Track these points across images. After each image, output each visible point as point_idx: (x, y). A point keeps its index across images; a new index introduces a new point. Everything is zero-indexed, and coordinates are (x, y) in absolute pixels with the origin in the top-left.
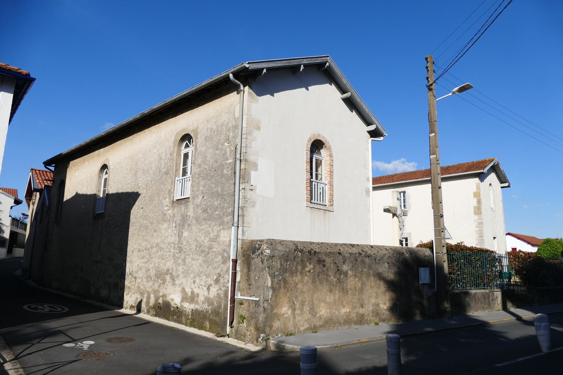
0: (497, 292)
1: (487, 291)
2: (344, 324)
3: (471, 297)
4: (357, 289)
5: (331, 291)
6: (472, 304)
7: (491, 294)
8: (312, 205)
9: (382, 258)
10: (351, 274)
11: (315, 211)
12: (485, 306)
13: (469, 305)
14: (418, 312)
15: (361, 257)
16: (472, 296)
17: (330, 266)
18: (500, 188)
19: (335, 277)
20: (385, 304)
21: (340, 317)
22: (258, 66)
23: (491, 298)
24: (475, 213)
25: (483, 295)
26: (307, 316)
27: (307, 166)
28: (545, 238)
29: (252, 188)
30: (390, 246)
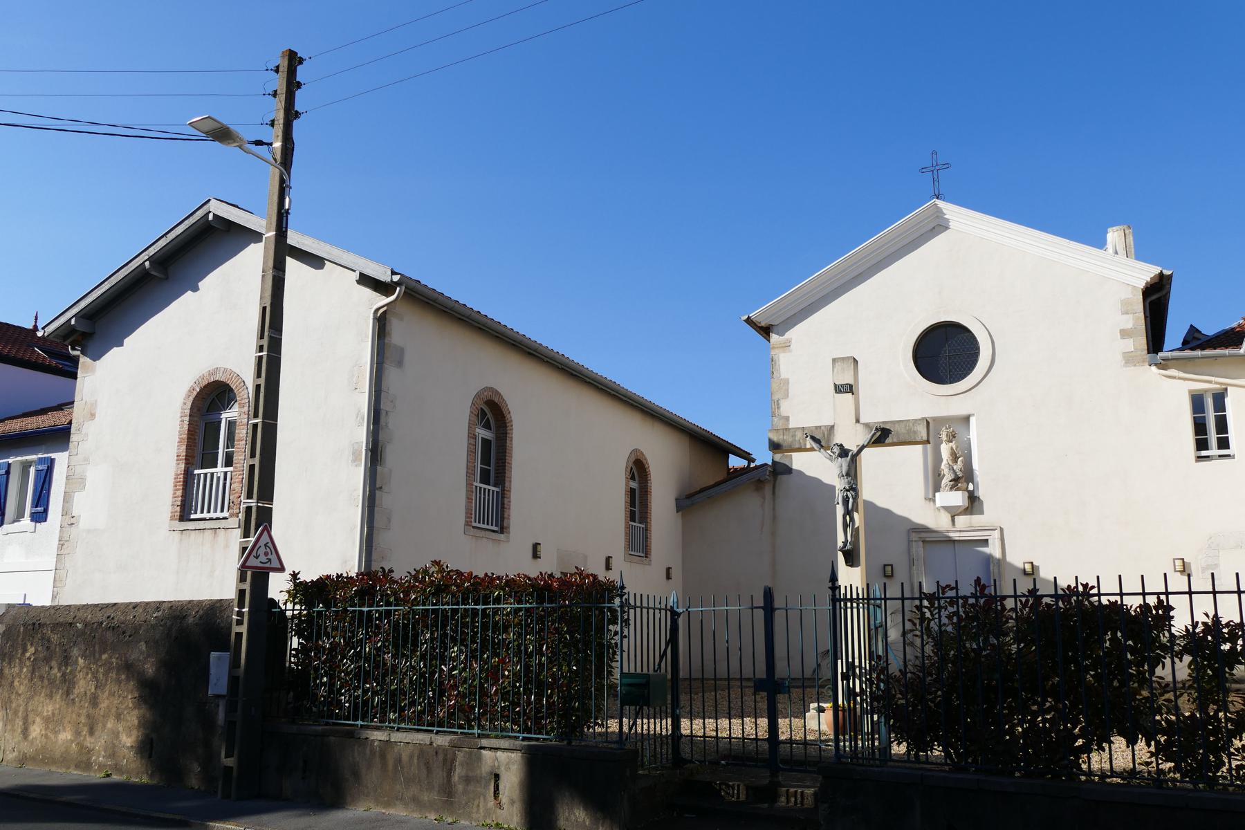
0: (499, 753)
1: (442, 741)
2: (113, 751)
3: (368, 752)
4: (88, 695)
5: (50, 696)
6: (371, 777)
7: (460, 756)
8: (190, 525)
9: (136, 630)
10: (83, 665)
11: (189, 536)
12: (425, 797)
13: (356, 775)
14: (196, 768)
15: (100, 631)
16: (371, 751)
17: (55, 649)
18: (832, 387)
19: (59, 669)
20: (129, 736)
21: (57, 747)
22: (1214, 443)
23: (458, 772)
24: (82, 480)
25: (425, 755)
26: (18, 736)
27: (498, 463)
28: (188, 599)
29: (73, 520)
30: (179, 601)
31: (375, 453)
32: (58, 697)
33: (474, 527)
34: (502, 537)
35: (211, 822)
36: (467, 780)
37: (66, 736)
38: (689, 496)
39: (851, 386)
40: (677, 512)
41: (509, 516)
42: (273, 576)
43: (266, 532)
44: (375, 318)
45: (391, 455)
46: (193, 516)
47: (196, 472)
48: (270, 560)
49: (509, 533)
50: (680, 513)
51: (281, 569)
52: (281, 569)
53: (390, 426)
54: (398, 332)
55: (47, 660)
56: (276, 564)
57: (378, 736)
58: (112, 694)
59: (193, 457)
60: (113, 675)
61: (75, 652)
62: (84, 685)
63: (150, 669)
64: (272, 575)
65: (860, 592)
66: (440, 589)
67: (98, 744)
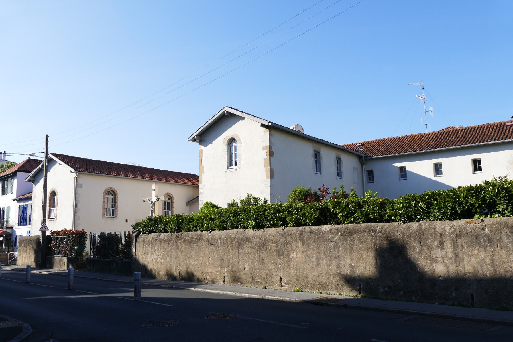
31: (76, 206)
32: (25, 253)
33: (105, 217)
34: (115, 218)
35: (191, 288)
36: (62, 263)
37: (26, 260)
38: (188, 202)
39: (155, 189)
40: (186, 206)
41: (117, 214)
42: (47, 231)
43: (44, 224)
44: (75, 179)
45: (79, 206)
46: (51, 218)
47: (51, 209)
48: (45, 229)
49: (117, 217)
50: (188, 206)
51: (48, 230)
52: (48, 230)
53: (79, 200)
54: (80, 181)
55: (24, 246)
56: (47, 229)
57: (55, 257)
58: (31, 252)
59: (51, 206)
60: (31, 249)
61: (27, 245)
62: (28, 251)
63: (35, 247)
64: (46, 231)
65: (130, 232)
66: (451, 191)
67: (30, 261)
